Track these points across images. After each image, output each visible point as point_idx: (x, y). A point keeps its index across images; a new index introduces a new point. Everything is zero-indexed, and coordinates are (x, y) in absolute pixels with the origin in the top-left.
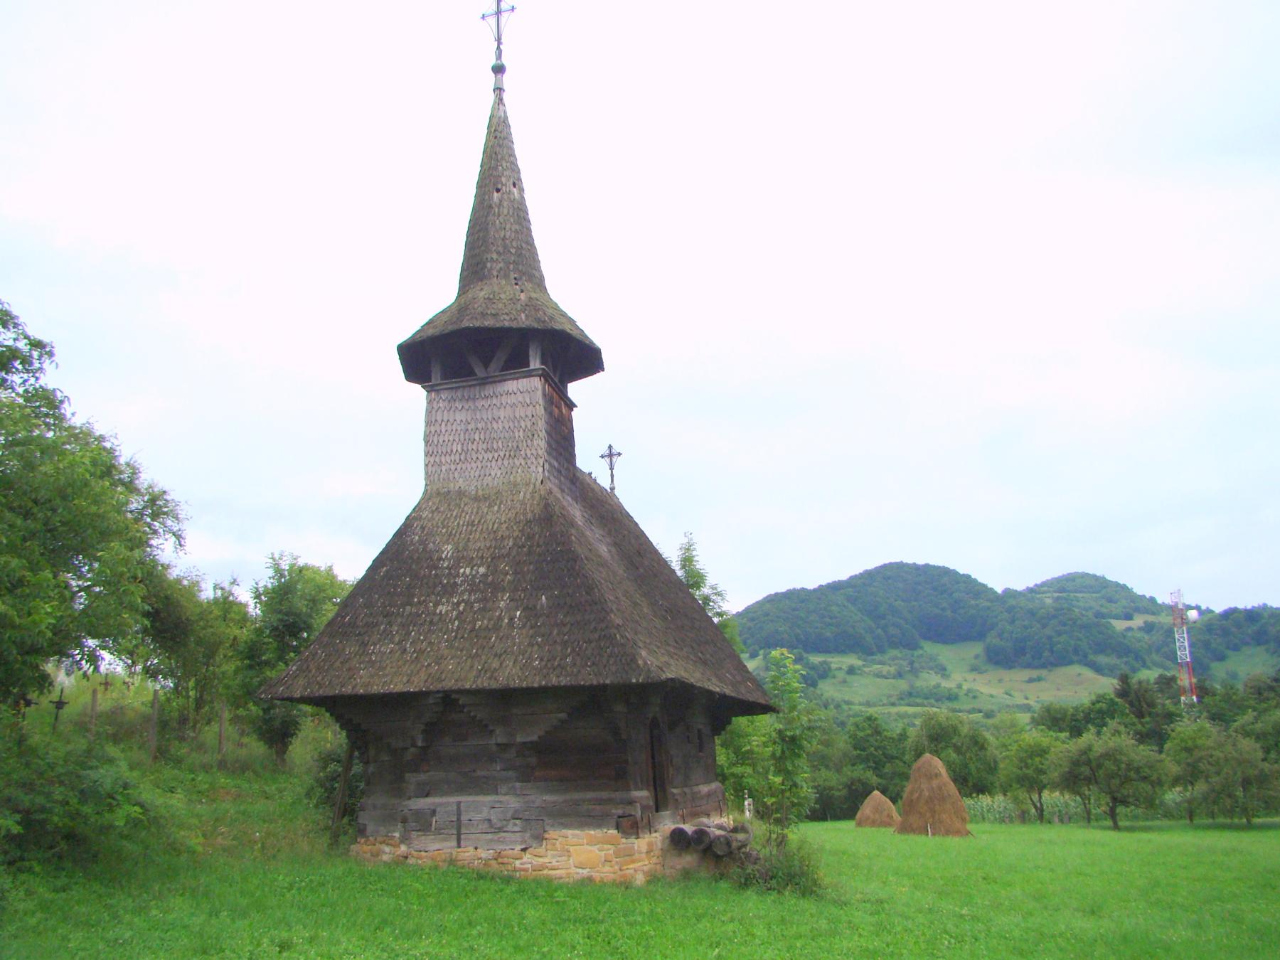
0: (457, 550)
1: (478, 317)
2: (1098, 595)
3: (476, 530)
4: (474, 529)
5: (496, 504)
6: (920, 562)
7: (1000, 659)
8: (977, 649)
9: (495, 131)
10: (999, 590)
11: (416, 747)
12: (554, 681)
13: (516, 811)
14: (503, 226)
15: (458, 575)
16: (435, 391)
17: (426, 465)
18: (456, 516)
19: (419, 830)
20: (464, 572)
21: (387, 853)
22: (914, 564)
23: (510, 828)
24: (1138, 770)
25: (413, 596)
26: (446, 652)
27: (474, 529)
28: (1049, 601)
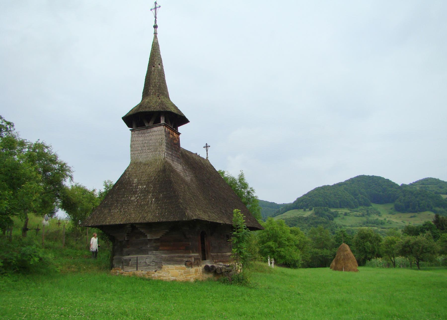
0: (138, 180)
6: (371, 175)
7: (400, 209)
8: (392, 206)
9: (154, 47)
10: (400, 184)
12: (162, 220)
14: (155, 78)
15: (138, 189)
17: (131, 154)
19: (126, 265)
20: (140, 187)
22: (368, 175)
24: (426, 249)
25: (125, 195)
26: (132, 212)
28: (418, 188)
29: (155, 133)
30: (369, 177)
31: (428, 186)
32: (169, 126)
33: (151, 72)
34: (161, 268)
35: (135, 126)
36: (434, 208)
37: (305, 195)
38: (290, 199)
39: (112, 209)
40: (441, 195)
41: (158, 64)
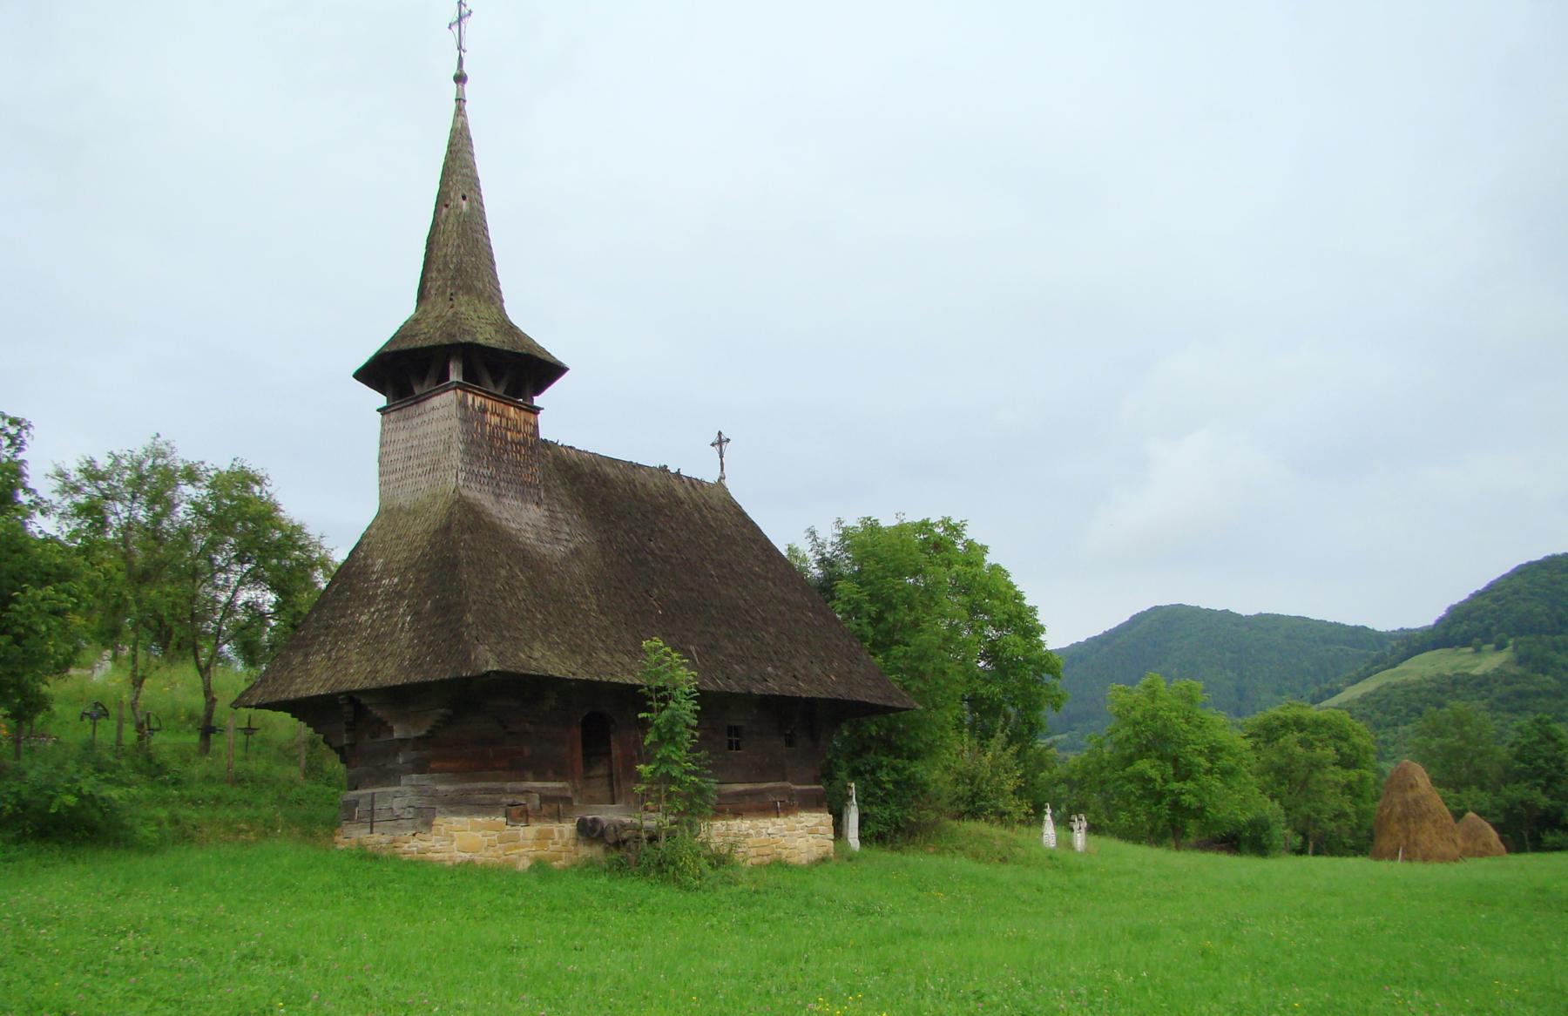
0: (385, 564)
17: (380, 485)
29: (436, 415)
32: (476, 389)
34: (428, 825)
37: (1479, 595)
38: (1423, 613)
41: (460, 196)
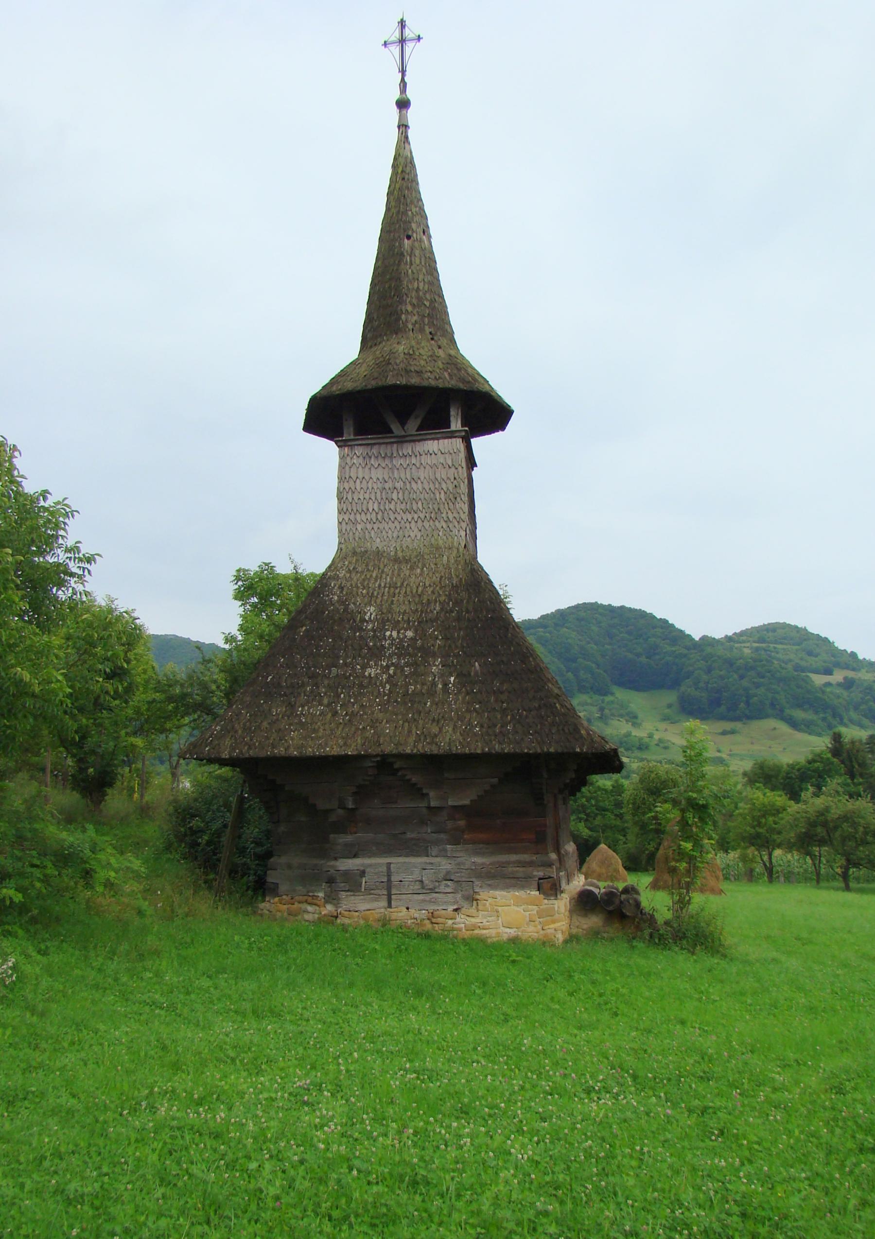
1: (403, 373)
2: (797, 647)
3: (399, 593)
4: (397, 591)
5: (418, 566)
6: (616, 604)
8: (671, 697)
9: (402, 172)
10: (697, 637)
11: (344, 808)
13: (448, 873)
16: (349, 446)
17: (340, 523)
18: (377, 576)
19: (348, 891)
20: (391, 635)
21: (311, 913)
22: (610, 605)
23: (442, 888)
26: (381, 715)
27: (397, 591)
28: (747, 651)
29: (427, 460)
30: (610, 609)
31: (780, 646)
33: (402, 254)
35: (352, 429)
36: (788, 711)
39: (298, 704)
40: (811, 675)
